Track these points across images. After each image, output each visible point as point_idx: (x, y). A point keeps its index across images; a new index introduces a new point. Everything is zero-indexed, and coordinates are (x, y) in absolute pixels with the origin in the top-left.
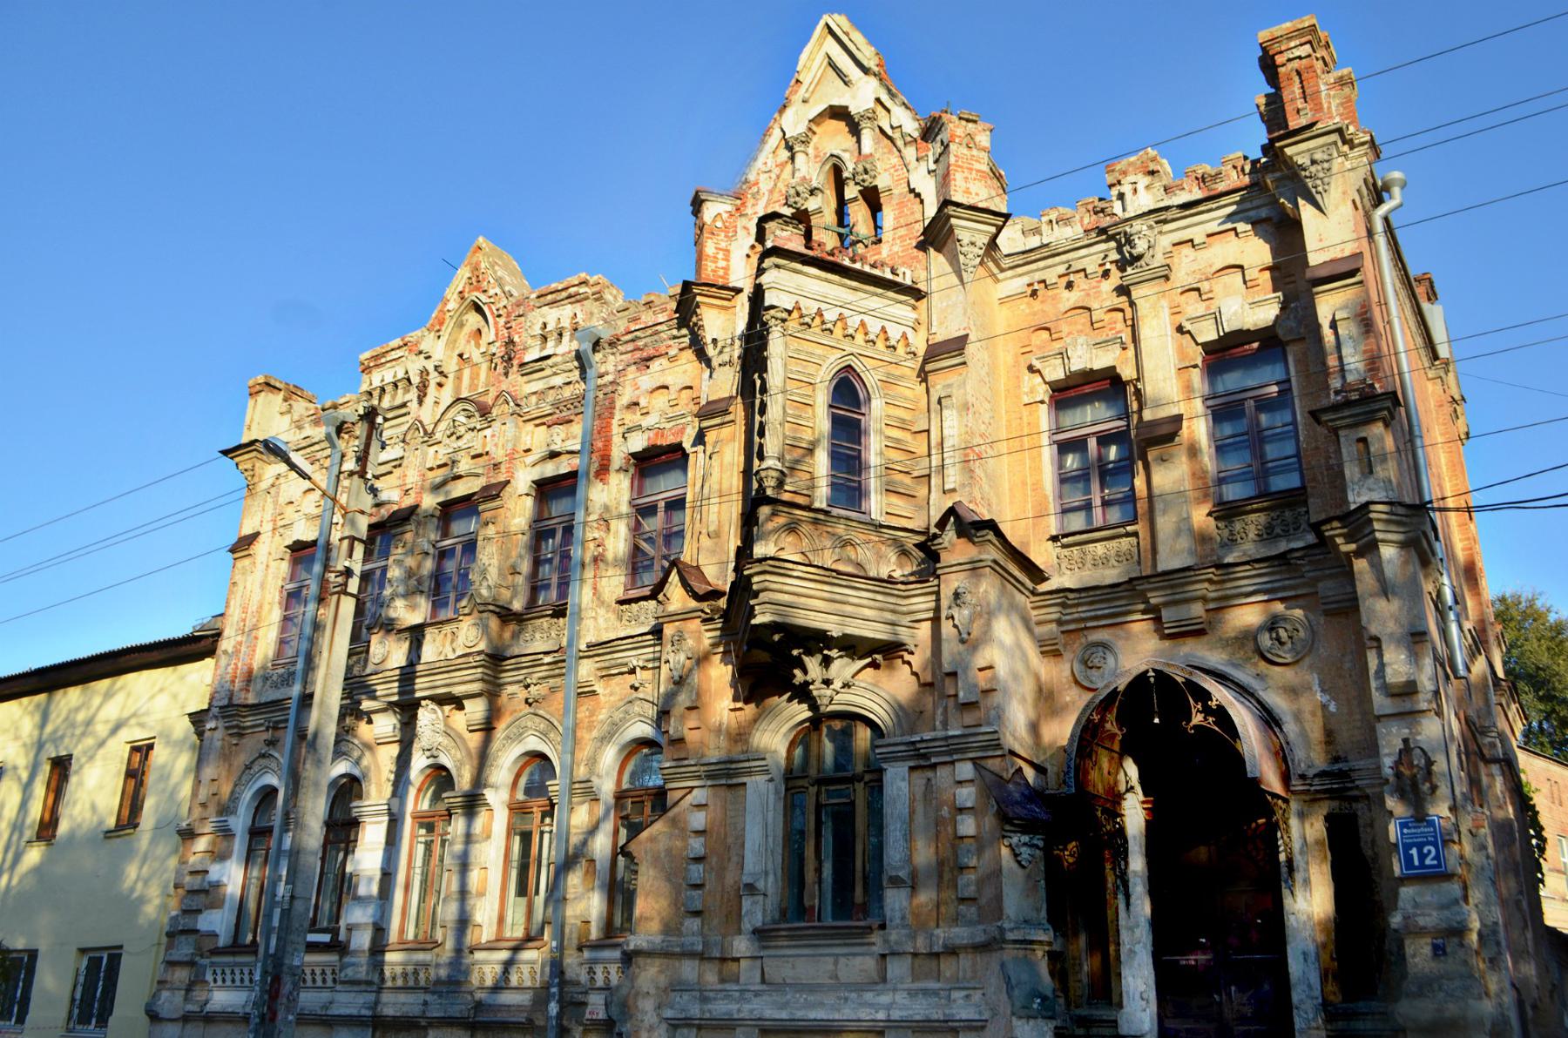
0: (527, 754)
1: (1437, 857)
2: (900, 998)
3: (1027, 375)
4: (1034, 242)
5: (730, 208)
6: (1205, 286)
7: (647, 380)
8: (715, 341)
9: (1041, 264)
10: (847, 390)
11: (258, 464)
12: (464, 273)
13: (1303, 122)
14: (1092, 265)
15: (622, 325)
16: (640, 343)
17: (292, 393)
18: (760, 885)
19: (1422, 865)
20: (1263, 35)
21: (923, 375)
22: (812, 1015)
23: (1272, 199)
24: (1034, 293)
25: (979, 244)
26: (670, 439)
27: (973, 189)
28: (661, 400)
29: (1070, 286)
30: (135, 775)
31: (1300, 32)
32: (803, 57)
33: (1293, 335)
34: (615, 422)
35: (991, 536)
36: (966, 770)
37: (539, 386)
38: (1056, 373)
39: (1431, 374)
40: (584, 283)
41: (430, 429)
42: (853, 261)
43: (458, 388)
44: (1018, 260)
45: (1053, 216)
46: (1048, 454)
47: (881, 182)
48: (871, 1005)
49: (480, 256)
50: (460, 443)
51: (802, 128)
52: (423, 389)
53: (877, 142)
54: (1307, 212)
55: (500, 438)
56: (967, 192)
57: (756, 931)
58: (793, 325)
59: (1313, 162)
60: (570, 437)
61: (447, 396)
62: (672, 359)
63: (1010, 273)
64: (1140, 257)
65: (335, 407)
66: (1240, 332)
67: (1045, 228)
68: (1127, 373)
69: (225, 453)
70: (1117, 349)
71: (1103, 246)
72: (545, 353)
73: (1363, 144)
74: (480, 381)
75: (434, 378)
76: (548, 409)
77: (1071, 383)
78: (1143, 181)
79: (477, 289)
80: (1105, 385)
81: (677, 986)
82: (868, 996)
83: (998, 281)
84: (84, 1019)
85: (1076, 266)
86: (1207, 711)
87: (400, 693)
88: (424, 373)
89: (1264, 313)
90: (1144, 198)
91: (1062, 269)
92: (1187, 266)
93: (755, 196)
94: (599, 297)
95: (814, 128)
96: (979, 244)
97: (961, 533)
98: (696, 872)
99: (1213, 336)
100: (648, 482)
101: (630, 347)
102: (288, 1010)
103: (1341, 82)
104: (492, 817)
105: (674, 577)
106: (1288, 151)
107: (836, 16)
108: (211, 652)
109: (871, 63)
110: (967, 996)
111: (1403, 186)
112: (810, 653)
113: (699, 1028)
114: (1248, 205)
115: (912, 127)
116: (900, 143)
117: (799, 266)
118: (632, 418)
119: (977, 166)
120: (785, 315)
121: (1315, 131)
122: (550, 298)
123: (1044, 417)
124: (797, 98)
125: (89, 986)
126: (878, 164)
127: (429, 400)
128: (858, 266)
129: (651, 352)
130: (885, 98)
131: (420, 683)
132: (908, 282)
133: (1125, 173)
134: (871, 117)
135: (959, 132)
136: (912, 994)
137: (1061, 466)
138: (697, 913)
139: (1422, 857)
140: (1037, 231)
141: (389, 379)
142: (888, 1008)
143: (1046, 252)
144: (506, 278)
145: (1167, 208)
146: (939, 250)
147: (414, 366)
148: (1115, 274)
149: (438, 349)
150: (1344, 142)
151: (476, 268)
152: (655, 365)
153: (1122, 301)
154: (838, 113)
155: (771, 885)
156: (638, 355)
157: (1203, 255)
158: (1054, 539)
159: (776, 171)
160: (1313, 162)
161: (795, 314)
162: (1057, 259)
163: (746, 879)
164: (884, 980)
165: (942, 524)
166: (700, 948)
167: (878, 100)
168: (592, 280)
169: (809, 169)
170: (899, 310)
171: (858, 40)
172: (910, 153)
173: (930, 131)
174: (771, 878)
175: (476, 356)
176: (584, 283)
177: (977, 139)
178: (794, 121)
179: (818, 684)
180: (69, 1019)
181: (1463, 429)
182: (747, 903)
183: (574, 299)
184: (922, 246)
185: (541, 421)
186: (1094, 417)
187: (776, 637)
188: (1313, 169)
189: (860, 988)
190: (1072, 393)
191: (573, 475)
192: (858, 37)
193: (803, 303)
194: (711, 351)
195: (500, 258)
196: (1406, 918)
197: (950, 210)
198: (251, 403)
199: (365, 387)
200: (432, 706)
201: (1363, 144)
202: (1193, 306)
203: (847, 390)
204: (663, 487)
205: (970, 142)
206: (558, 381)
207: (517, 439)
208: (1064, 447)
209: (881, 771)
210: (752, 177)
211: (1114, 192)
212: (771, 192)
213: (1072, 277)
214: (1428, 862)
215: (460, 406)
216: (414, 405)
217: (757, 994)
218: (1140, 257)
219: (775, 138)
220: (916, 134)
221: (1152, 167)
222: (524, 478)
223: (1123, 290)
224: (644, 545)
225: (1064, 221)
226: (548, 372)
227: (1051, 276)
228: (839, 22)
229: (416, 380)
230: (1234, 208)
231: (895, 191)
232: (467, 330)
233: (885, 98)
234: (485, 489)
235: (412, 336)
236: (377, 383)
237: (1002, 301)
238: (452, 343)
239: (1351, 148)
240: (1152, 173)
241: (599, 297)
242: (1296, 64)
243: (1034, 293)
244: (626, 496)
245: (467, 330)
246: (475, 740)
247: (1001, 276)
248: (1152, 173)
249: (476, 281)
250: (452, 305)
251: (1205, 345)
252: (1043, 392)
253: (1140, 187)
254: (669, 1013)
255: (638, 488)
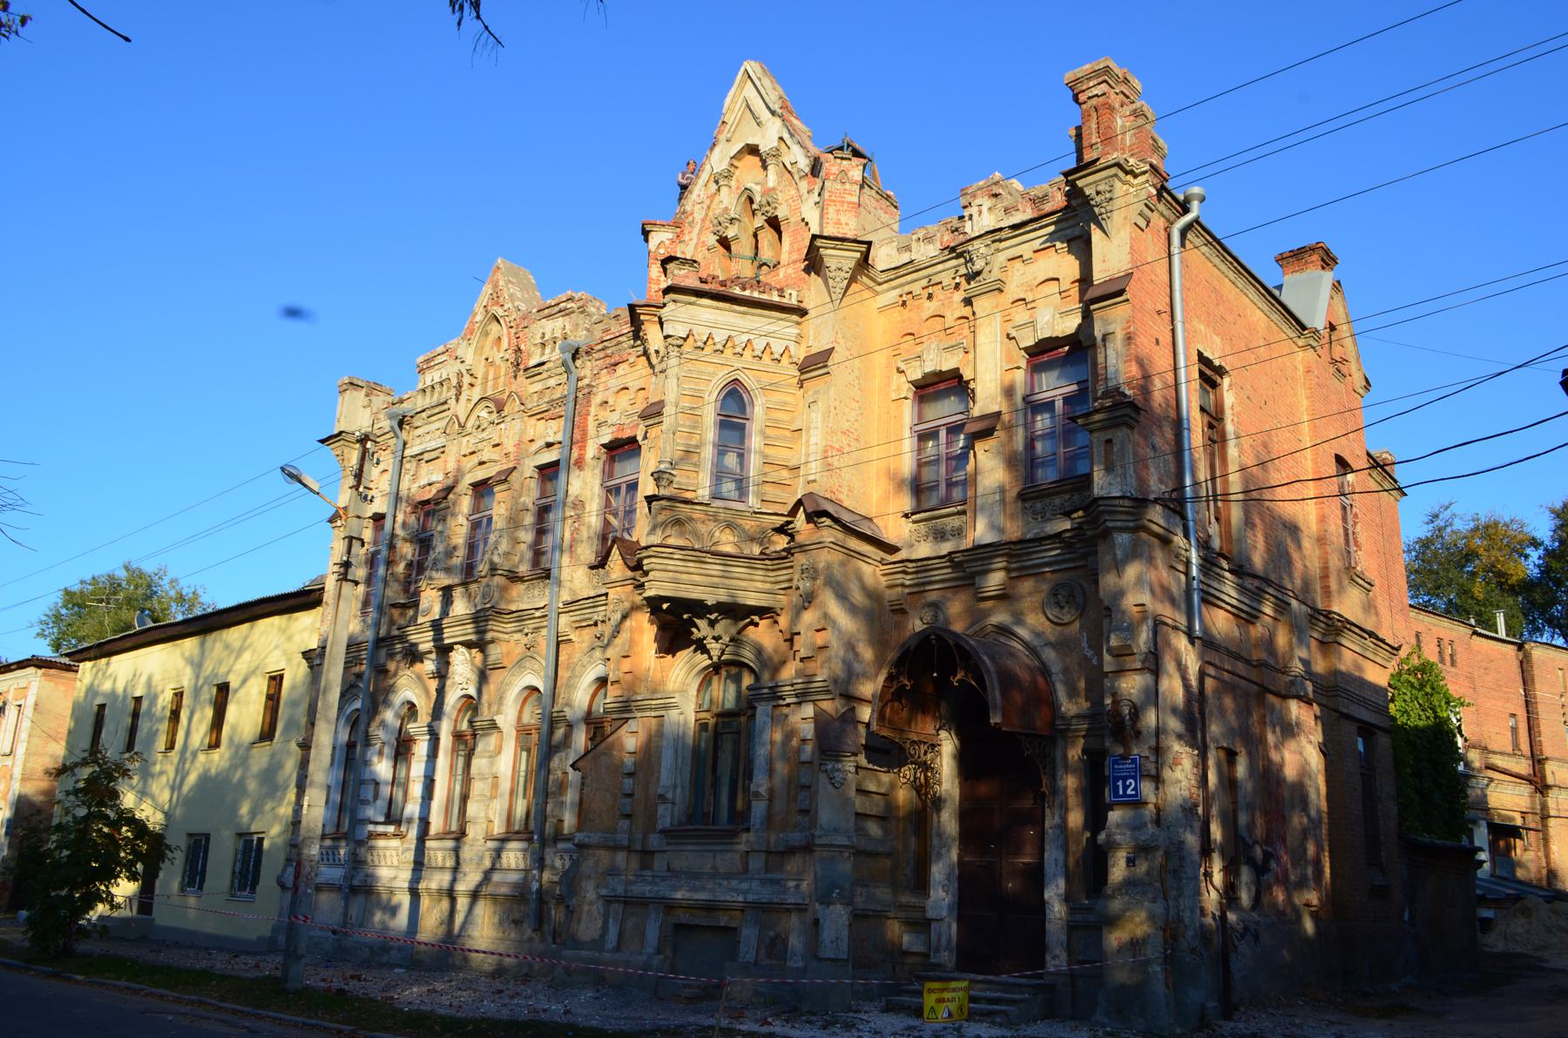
0: (527, 688)
1: (1135, 789)
2: (755, 885)
3: (896, 375)
4: (905, 258)
5: (670, 236)
6: (1029, 298)
7: (614, 382)
8: (657, 352)
9: (909, 278)
10: (735, 397)
11: (346, 450)
12: (487, 289)
13: (1095, 155)
14: (946, 278)
15: (598, 335)
16: (609, 352)
17: (372, 389)
18: (670, 796)
19: (1125, 795)
20: (1069, 76)
21: (801, 384)
22: (697, 896)
23: (1075, 222)
24: (904, 303)
25: (845, 268)
26: (626, 434)
27: (843, 219)
28: (623, 401)
29: (930, 297)
30: (273, 699)
31: (1096, 73)
32: (728, 100)
33: (1077, 350)
34: (590, 418)
35: (828, 522)
36: (808, 710)
37: (538, 387)
38: (917, 375)
39: (1301, 342)
40: (570, 299)
41: (462, 420)
42: (744, 289)
43: (485, 390)
44: (891, 275)
45: (921, 234)
46: (908, 444)
47: (781, 213)
48: (736, 890)
49: (499, 275)
50: (484, 435)
51: (724, 165)
52: (459, 386)
53: (780, 176)
54: (1096, 235)
55: (512, 431)
56: (838, 223)
57: (662, 831)
58: (687, 347)
59: (1098, 193)
60: (553, 430)
61: (476, 394)
62: (632, 365)
63: (885, 286)
64: (978, 273)
65: (401, 402)
66: (1050, 338)
67: (914, 245)
68: (967, 374)
69: (323, 441)
70: (962, 354)
71: (954, 262)
72: (544, 359)
73: (1144, 173)
74: (500, 381)
75: (467, 379)
76: (544, 407)
77: (929, 381)
78: (987, 203)
79: (497, 303)
80: (955, 383)
81: (612, 871)
82: (734, 883)
83: (877, 293)
84: (242, 888)
85: (935, 279)
87: (434, 640)
88: (460, 375)
89: (1071, 324)
90: (985, 218)
91: (924, 282)
92: (1019, 280)
93: (691, 224)
94: (582, 310)
95: (736, 163)
96: (845, 268)
97: (810, 518)
98: (628, 782)
99: (1030, 342)
100: (617, 466)
101: (601, 354)
102: (307, 885)
103: (1137, 114)
104: (502, 739)
105: (615, 551)
106: (1080, 183)
107: (753, 63)
108: (317, 603)
109: (776, 107)
110: (797, 886)
111: (1202, 199)
112: (700, 618)
113: (626, 903)
114: (1064, 225)
115: (804, 164)
116: (796, 177)
117: (693, 299)
118: (604, 415)
119: (849, 198)
120: (680, 342)
121: (1099, 165)
122: (547, 312)
123: (907, 410)
124: (722, 137)
125: (245, 863)
126: (780, 197)
127: (463, 398)
128: (747, 293)
129: (616, 358)
130: (786, 136)
131: (447, 633)
132: (794, 302)
133: (974, 196)
134: (776, 154)
135: (834, 170)
136: (763, 882)
137: (919, 450)
138: (628, 816)
139: (1125, 788)
140: (908, 248)
141: (437, 379)
142: (745, 893)
143: (909, 267)
144: (516, 290)
145: (1000, 229)
146: (818, 274)
147: (450, 370)
148: (964, 285)
149: (468, 353)
150: (1127, 173)
151: (496, 286)
152: (621, 369)
153: (967, 311)
154: (753, 150)
155: (679, 795)
156: (608, 361)
157: (1032, 268)
158: (906, 516)
159: (707, 202)
160: (1098, 193)
161: (691, 339)
162: (921, 274)
163: (660, 791)
164: (746, 870)
165: (793, 512)
166: (626, 843)
167: (781, 138)
168: (577, 297)
169: (728, 200)
170: (780, 329)
171: (767, 83)
172: (804, 185)
173: (816, 168)
174: (679, 790)
175: (497, 356)
176: (570, 299)
177: (851, 174)
178: (718, 160)
179: (709, 640)
180: (232, 886)
181: (1359, 383)
182: (661, 809)
183: (564, 312)
184: (807, 270)
185: (540, 415)
186: (945, 410)
187: (665, 606)
188: (1098, 199)
189: (728, 876)
190: (931, 390)
191: (556, 464)
192: (767, 82)
193: (696, 330)
194: (654, 360)
195: (516, 275)
196: (1108, 836)
197: (819, 242)
198: (340, 399)
199: (420, 386)
200: (462, 649)
201: (1144, 173)
202: (1020, 315)
203: (735, 397)
204: (624, 472)
205: (843, 176)
206: (552, 382)
207: (523, 432)
208: (923, 437)
209: (755, 708)
210: (688, 208)
211: (966, 213)
212: (703, 220)
213: (930, 290)
215: (484, 404)
216: (452, 402)
217: (663, 878)
218: (978, 273)
219: (705, 176)
220: (807, 170)
221: (996, 190)
222: (529, 468)
223: (968, 302)
224: (611, 519)
225: (928, 239)
226: (545, 375)
227: (916, 288)
228: (751, 66)
229: (454, 382)
230: (1052, 228)
231: (792, 220)
232: (491, 337)
233: (786, 136)
234: (499, 473)
235: (452, 344)
236: (429, 383)
237: (881, 310)
238: (479, 349)
239: (1136, 176)
240: (996, 195)
241: (582, 310)
242: (1094, 102)
243: (904, 303)
244: (598, 482)
245: (491, 337)
246: (433, 685)
247: (878, 288)
248: (996, 195)
249: (496, 298)
250: (479, 318)
251: (1026, 349)
252: (908, 390)
253: (985, 209)
254: (604, 892)
255: (608, 474)
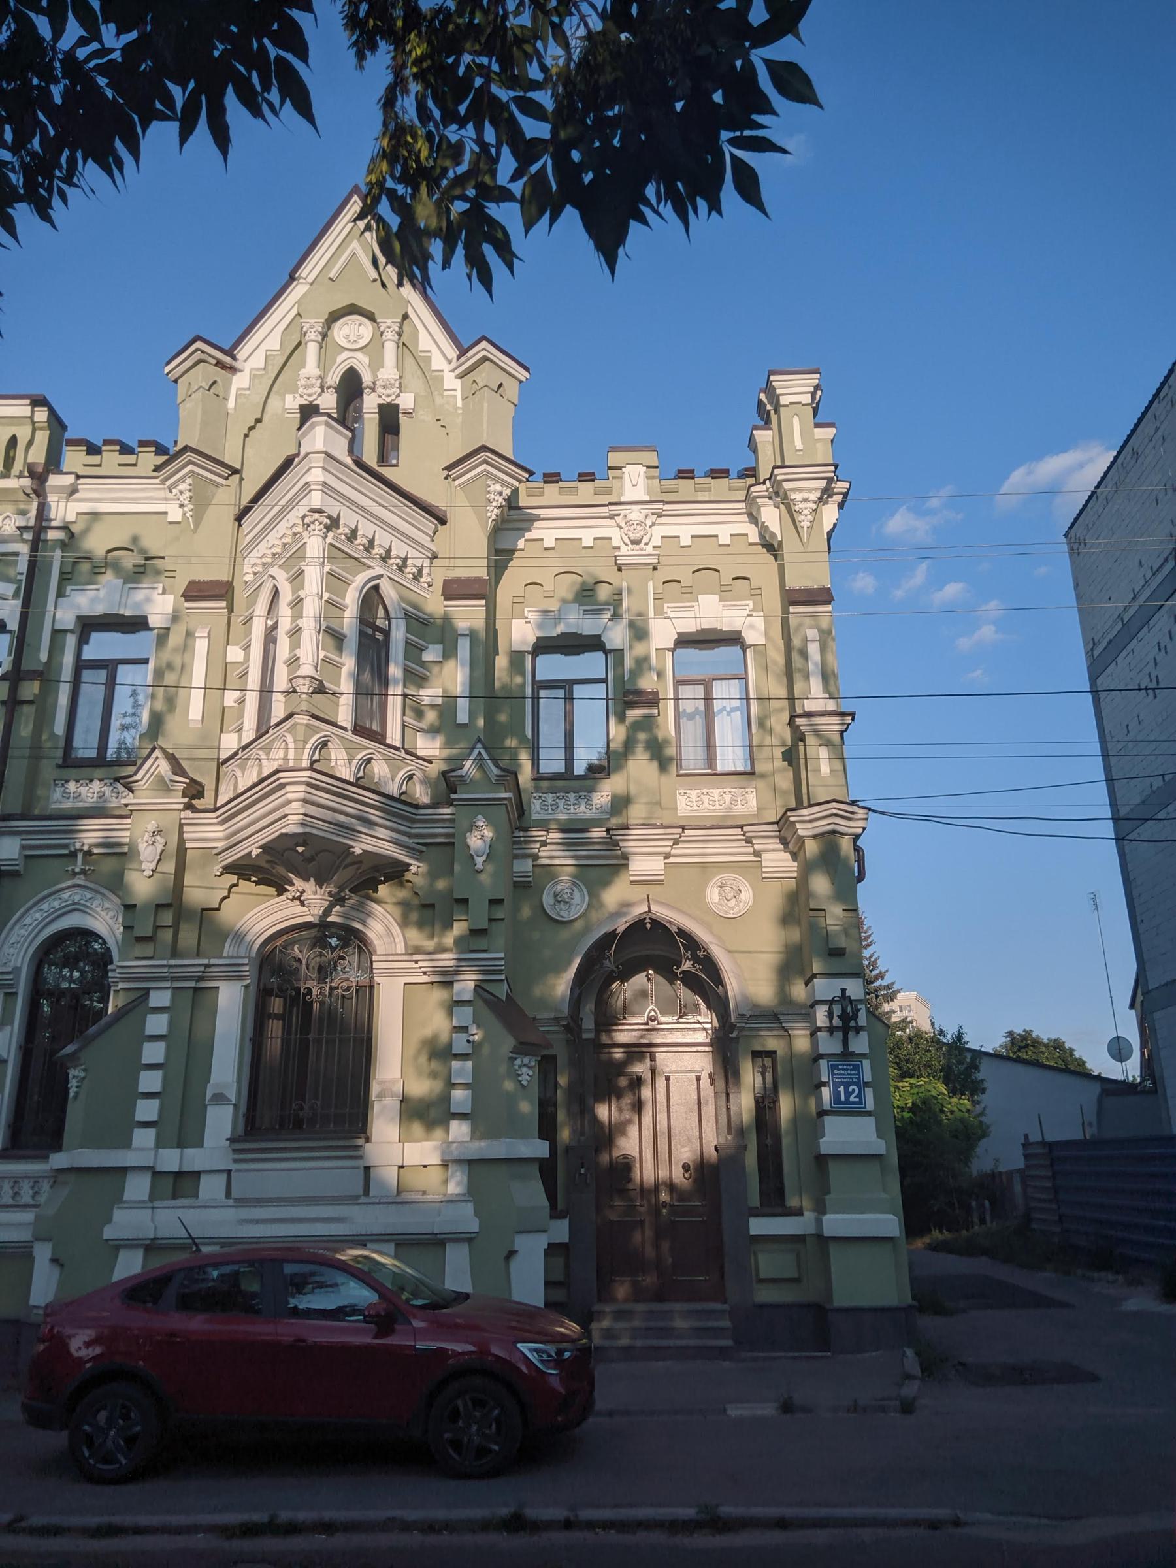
86: (695, 959)
139: (848, 1094)
214: (852, 1099)
